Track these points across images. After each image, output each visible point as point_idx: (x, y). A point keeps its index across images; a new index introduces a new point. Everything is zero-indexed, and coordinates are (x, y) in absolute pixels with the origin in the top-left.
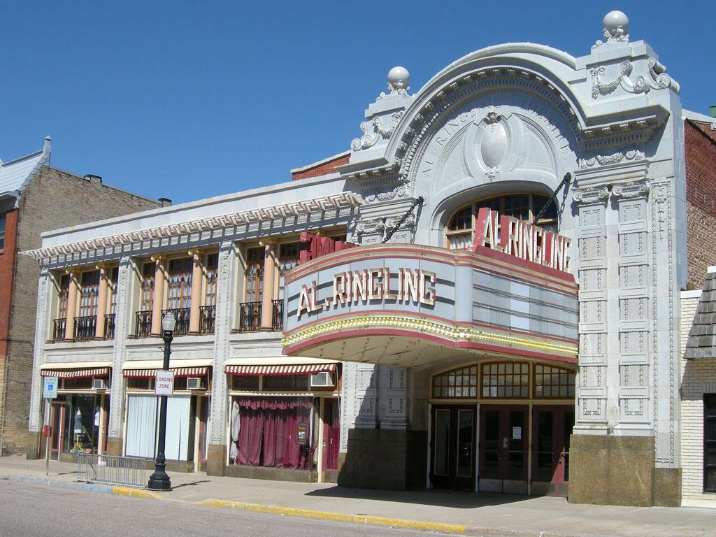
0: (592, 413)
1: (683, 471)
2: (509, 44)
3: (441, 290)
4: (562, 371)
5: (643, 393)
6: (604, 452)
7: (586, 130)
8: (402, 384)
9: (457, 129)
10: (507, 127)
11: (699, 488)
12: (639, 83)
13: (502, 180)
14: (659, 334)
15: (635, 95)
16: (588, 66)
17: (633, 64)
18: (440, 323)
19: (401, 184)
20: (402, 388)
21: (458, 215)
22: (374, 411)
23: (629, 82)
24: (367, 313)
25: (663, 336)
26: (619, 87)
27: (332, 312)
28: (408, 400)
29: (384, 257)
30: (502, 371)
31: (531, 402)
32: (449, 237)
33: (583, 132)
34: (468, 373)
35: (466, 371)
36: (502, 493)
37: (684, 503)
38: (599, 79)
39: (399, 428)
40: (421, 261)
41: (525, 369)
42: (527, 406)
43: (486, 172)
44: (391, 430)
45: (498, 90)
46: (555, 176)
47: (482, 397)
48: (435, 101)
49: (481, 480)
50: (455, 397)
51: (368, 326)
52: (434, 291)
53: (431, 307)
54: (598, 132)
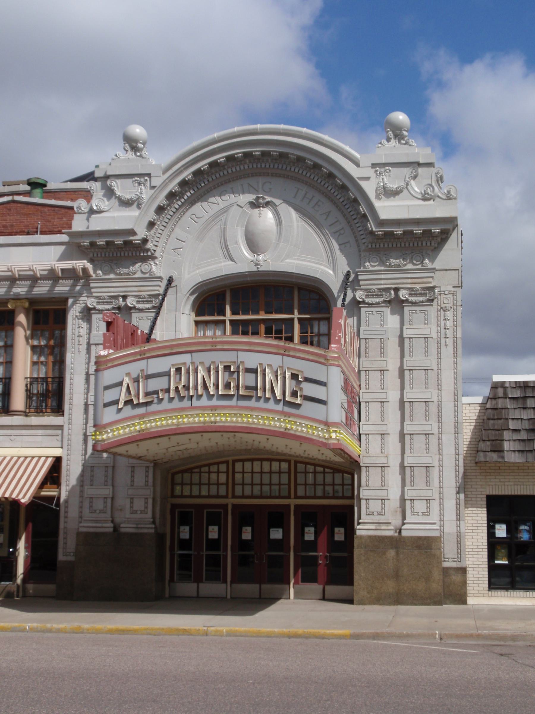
0: (375, 513)
1: (468, 569)
2: (305, 130)
3: (309, 389)
4: (327, 470)
5: (428, 494)
6: (391, 553)
7: (377, 232)
8: (147, 481)
9: (216, 208)
10: (277, 215)
11: (484, 585)
12: (429, 191)
13: (270, 270)
14: (444, 437)
15: (421, 202)
16: (374, 165)
17: (421, 170)
18: (309, 423)
19: (145, 259)
20: (148, 486)
21: (211, 300)
22: (109, 512)
23: (416, 188)
24: (214, 408)
25: (448, 439)
26: (405, 191)
27: (165, 405)
28: (154, 499)
29: (237, 350)
30: (257, 468)
31: (293, 502)
32: (197, 323)
33: (372, 233)
34: (216, 470)
35: (214, 468)
36: (198, 597)
37: (470, 601)
38: (385, 179)
39: (146, 531)
40: (284, 357)
41: (223, 468)
42: (288, 506)
43: (252, 258)
44: (135, 534)
45: (269, 173)
46: (331, 272)
47: (173, 496)
48: (198, 173)
49: (234, 585)
50: (200, 496)
51: (215, 422)
52: (301, 389)
53: (298, 406)
54: (389, 235)
